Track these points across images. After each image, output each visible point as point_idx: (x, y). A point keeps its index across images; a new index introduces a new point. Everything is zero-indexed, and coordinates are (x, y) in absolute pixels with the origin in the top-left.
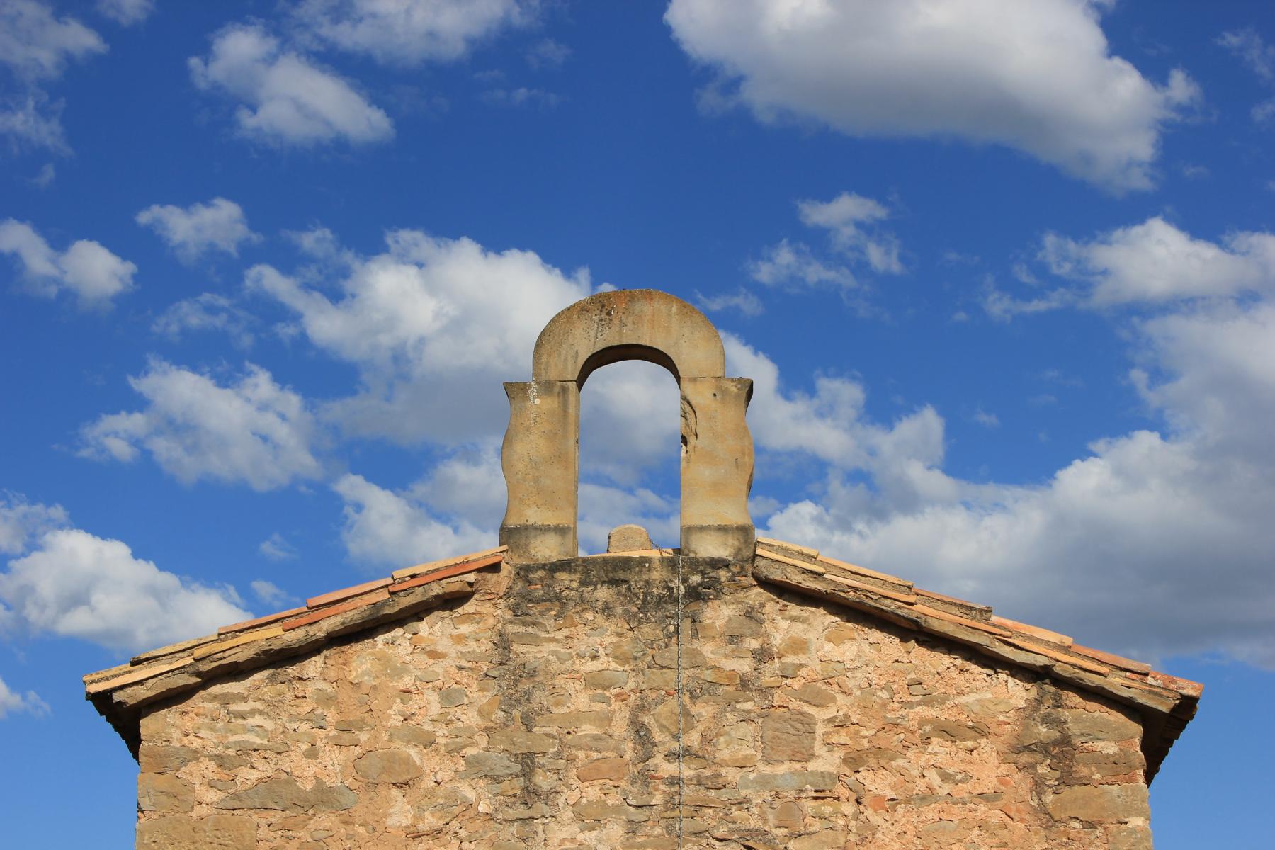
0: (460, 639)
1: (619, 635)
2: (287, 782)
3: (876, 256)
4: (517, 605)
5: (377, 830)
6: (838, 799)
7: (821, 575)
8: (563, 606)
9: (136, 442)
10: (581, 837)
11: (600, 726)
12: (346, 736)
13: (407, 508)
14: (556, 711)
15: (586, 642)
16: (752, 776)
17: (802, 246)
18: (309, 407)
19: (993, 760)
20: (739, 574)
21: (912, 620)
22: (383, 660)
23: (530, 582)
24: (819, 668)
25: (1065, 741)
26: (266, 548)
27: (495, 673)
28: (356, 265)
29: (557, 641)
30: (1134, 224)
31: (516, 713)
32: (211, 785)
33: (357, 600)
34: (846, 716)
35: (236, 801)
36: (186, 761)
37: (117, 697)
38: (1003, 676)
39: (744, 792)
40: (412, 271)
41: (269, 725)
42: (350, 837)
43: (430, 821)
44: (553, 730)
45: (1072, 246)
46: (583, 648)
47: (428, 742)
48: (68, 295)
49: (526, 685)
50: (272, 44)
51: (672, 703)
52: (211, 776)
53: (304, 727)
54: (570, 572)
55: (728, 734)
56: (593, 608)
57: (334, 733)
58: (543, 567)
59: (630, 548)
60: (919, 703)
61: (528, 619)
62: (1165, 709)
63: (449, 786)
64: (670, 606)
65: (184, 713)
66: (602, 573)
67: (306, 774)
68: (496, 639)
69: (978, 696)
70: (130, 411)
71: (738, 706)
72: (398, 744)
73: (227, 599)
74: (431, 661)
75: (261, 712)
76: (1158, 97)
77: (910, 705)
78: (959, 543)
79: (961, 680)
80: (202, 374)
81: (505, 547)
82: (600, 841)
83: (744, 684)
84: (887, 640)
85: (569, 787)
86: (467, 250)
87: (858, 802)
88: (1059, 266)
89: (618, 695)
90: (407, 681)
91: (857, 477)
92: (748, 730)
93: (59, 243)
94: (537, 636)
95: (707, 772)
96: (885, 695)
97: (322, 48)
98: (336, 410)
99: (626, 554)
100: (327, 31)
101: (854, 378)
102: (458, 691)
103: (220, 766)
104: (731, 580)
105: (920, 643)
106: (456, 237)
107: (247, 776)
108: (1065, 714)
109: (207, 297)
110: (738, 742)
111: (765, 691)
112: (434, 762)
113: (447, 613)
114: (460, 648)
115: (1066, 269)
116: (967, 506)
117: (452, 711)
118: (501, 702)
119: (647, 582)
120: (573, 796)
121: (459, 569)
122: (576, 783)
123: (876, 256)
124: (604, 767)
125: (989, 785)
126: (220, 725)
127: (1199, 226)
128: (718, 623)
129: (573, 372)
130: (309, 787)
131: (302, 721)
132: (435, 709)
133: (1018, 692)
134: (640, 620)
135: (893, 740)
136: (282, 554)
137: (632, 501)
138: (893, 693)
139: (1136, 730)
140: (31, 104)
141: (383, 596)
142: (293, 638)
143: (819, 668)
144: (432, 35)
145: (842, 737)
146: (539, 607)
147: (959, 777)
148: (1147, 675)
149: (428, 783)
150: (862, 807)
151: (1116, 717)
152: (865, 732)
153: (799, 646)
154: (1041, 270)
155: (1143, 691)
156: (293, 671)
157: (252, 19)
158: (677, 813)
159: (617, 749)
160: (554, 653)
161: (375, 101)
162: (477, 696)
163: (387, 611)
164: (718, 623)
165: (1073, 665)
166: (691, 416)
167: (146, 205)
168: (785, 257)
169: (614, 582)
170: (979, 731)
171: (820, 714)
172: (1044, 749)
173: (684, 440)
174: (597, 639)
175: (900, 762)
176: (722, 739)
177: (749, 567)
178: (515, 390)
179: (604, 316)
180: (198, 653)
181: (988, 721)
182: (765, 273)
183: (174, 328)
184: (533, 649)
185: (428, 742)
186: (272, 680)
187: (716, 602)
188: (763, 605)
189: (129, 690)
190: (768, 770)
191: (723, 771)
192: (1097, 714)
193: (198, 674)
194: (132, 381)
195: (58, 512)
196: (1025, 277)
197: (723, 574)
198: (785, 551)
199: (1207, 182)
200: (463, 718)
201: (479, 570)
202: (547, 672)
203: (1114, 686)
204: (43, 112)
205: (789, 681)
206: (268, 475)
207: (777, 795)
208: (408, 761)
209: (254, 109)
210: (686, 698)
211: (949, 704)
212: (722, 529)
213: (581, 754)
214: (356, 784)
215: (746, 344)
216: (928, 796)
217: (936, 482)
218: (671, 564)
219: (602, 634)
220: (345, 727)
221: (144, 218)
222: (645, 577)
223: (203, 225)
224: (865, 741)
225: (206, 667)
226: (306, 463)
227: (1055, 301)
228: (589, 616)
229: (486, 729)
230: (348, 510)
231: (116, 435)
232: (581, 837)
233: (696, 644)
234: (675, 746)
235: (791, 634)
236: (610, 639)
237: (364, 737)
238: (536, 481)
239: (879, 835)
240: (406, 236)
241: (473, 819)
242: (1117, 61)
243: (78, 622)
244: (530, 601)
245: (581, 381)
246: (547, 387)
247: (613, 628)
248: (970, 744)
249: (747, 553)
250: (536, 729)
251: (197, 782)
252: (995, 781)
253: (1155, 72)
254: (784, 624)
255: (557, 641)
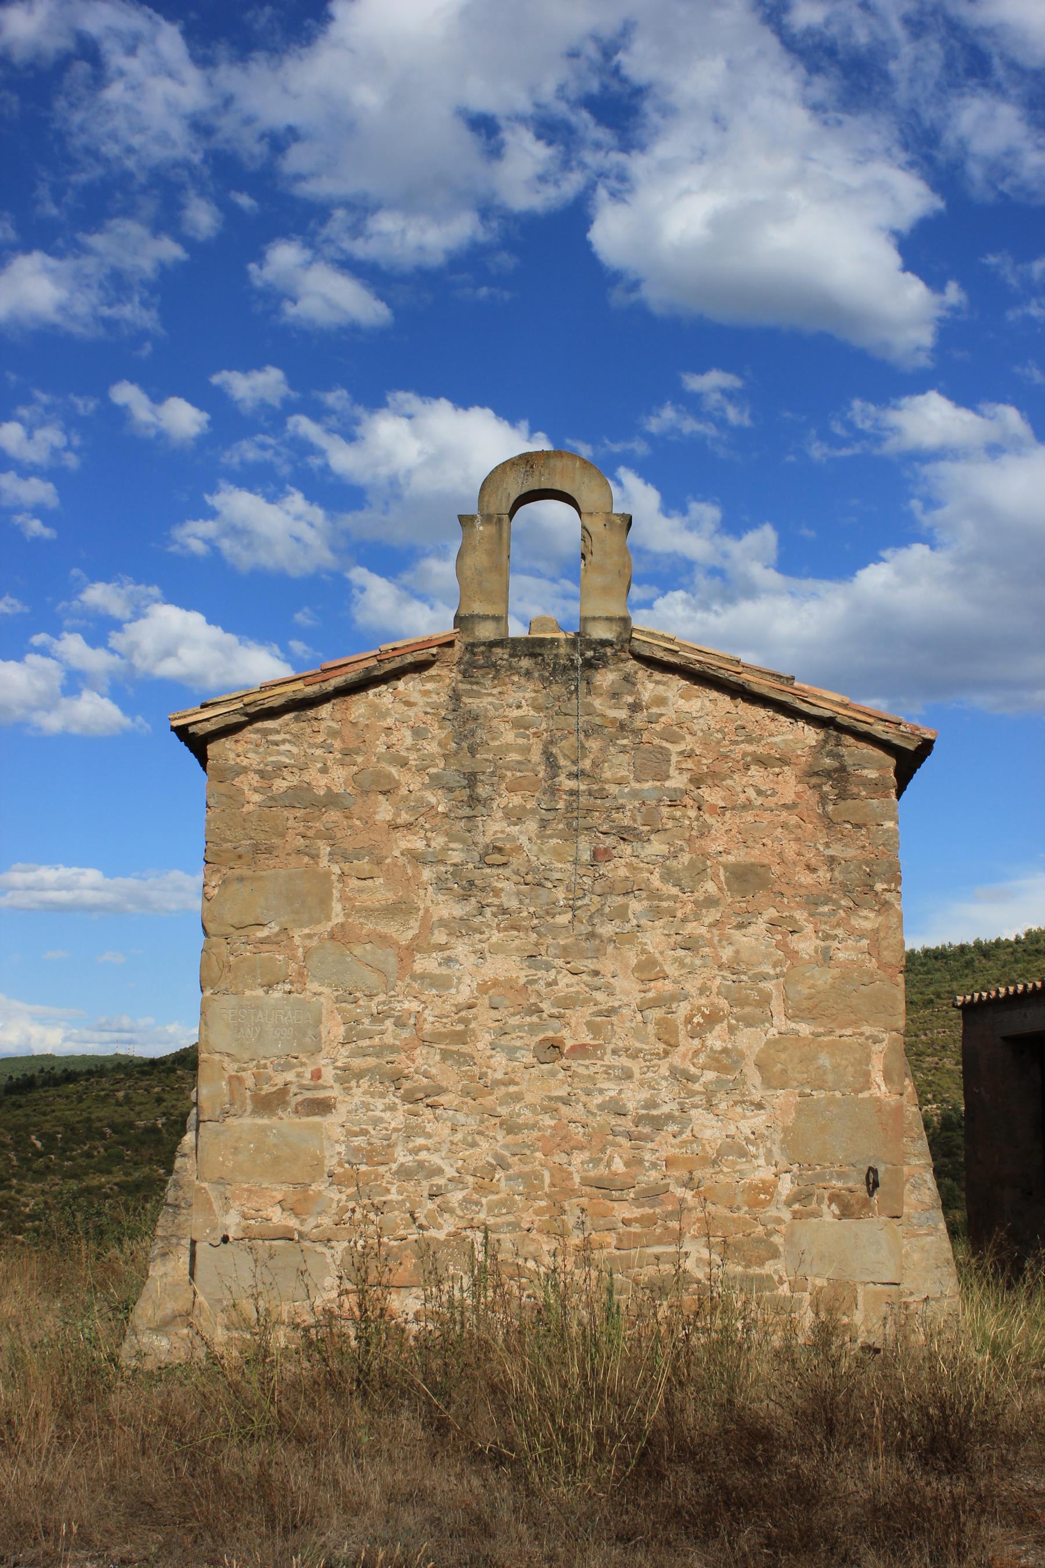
0: (426, 693)
1: (536, 691)
2: (307, 789)
3: (732, 414)
4: (466, 670)
5: (368, 822)
6: (685, 806)
7: (677, 652)
8: (498, 671)
9: (207, 541)
10: (508, 829)
11: (523, 755)
12: (347, 758)
13: (397, 592)
14: (492, 744)
15: (513, 696)
16: (626, 790)
17: (681, 407)
18: (331, 518)
19: (793, 781)
20: (620, 650)
21: (739, 684)
22: (374, 707)
23: (475, 655)
24: (674, 716)
25: (842, 769)
26: (299, 617)
27: (450, 717)
28: (365, 416)
29: (493, 695)
30: (918, 394)
31: (465, 745)
32: (256, 790)
33: (355, 665)
34: (692, 750)
35: (273, 802)
36: (238, 774)
37: (191, 729)
38: (801, 724)
39: (621, 801)
40: (404, 422)
41: (295, 750)
42: (350, 827)
43: (405, 817)
44: (490, 757)
45: (872, 408)
46: (511, 700)
47: (404, 763)
48: (162, 435)
49: (471, 725)
50: (308, 254)
51: (572, 739)
52: (255, 784)
53: (319, 752)
54: (502, 648)
55: (610, 761)
56: (518, 673)
57: (340, 756)
58: (484, 644)
59: (544, 632)
60: (742, 742)
61: (473, 680)
62: (911, 748)
63: (418, 794)
64: (571, 672)
65: (237, 741)
66: (525, 649)
67: (320, 784)
68: (451, 693)
69: (783, 737)
70: (206, 519)
71: (618, 742)
72: (384, 765)
73: (272, 655)
74: (406, 708)
75: (289, 742)
76: (936, 299)
77: (736, 743)
78: (784, 622)
79: (772, 726)
80: (256, 494)
81: (458, 630)
82: (521, 833)
83: (622, 726)
84: (721, 698)
85: (500, 796)
86: (444, 406)
87: (699, 809)
88: (863, 421)
89: (534, 733)
90: (389, 722)
91: (715, 572)
92: (624, 758)
93: (157, 399)
94: (480, 692)
95: (595, 787)
96: (720, 736)
97: (343, 258)
98: (349, 520)
99: (542, 636)
100: (347, 244)
101: (714, 503)
102: (425, 729)
103: (262, 778)
104: (615, 655)
105: (744, 700)
106: (437, 396)
107: (280, 785)
108: (843, 751)
109: (260, 438)
110: (618, 767)
111: (638, 732)
112: (407, 777)
113: (416, 675)
114: (426, 699)
115: (866, 425)
116: (792, 594)
117: (420, 742)
118: (454, 737)
119: (556, 656)
120: (504, 802)
121: (427, 644)
122: (506, 793)
123: (732, 414)
124: (525, 782)
125: (789, 798)
126: (261, 750)
127: (965, 396)
128: (605, 684)
129: (506, 508)
130: (322, 793)
131: (317, 748)
132: (409, 741)
133: (811, 735)
134: (551, 682)
135: (724, 767)
136: (309, 622)
137: (556, 587)
138: (725, 734)
139: (891, 762)
140: (137, 299)
141: (373, 663)
142: (311, 690)
143: (674, 716)
144: (421, 249)
145: (689, 764)
146: (481, 672)
147: (769, 792)
148: (900, 724)
149: (404, 791)
150: (701, 813)
151: (878, 753)
152: (704, 761)
153: (661, 701)
154: (849, 425)
155: (897, 735)
156: (311, 713)
157: (294, 236)
158: (575, 814)
159: (533, 770)
160: (491, 703)
161: (381, 297)
162: (437, 732)
163: (376, 673)
164: (605, 684)
165: (849, 717)
166: (588, 540)
167: (217, 370)
168: (668, 414)
169: (533, 655)
170: (784, 761)
171: (674, 748)
172: (828, 774)
173: (583, 557)
174: (521, 694)
175: (729, 782)
176: (606, 764)
177: (626, 646)
178: (466, 521)
179: (528, 469)
180: (246, 700)
181: (789, 755)
182: (653, 426)
183: (236, 460)
184: (477, 701)
185: (404, 763)
186: (297, 719)
187: (604, 670)
188: (636, 673)
189: (200, 725)
190: (637, 786)
191: (607, 787)
192: (865, 751)
193: (246, 714)
194: (207, 497)
195: (155, 591)
196: (838, 429)
197: (609, 651)
198: (652, 635)
199: (966, 365)
200: (428, 747)
201: (439, 646)
202: (486, 717)
203: (877, 731)
204: (145, 304)
205: (653, 725)
206: (301, 565)
207: (644, 803)
208: (389, 776)
209: (295, 301)
210: (582, 736)
211: (763, 742)
212: (609, 619)
213: (509, 774)
214: (355, 792)
215: (639, 477)
216: (748, 806)
217: (772, 578)
218: (572, 643)
219: (524, 691)
220: (346, 753)
221: (216, 380)
222: (555, 652)
223: (256, 386)
224: (705, 767)
225: (251, 710)
226: (327, 558)
227: (856, 450)
228: (516, 678)
229: (443, 755)
230: (355, 592)
231: (194, 536)
232: (508, 829)
233: (589, 699)
234: (574, 769)
235: (656, 693)
236: (529, 695)
237: (360, 759)
238: (480, 583)
239: (713, 831)
240: (401, 396)
241: (434, 817)
242: (909, 276)
243: (169, 668)
244: (475, 668)
245: (511, 514)
246: (488, 519)
247: (532, 687)
248: (777, 770)
249: (626, 636)
250: (478, 756)
251: (246, 788)
252: (793, 796)
253: (935, 282)
254: (650, 686)
255: (493, 695)
